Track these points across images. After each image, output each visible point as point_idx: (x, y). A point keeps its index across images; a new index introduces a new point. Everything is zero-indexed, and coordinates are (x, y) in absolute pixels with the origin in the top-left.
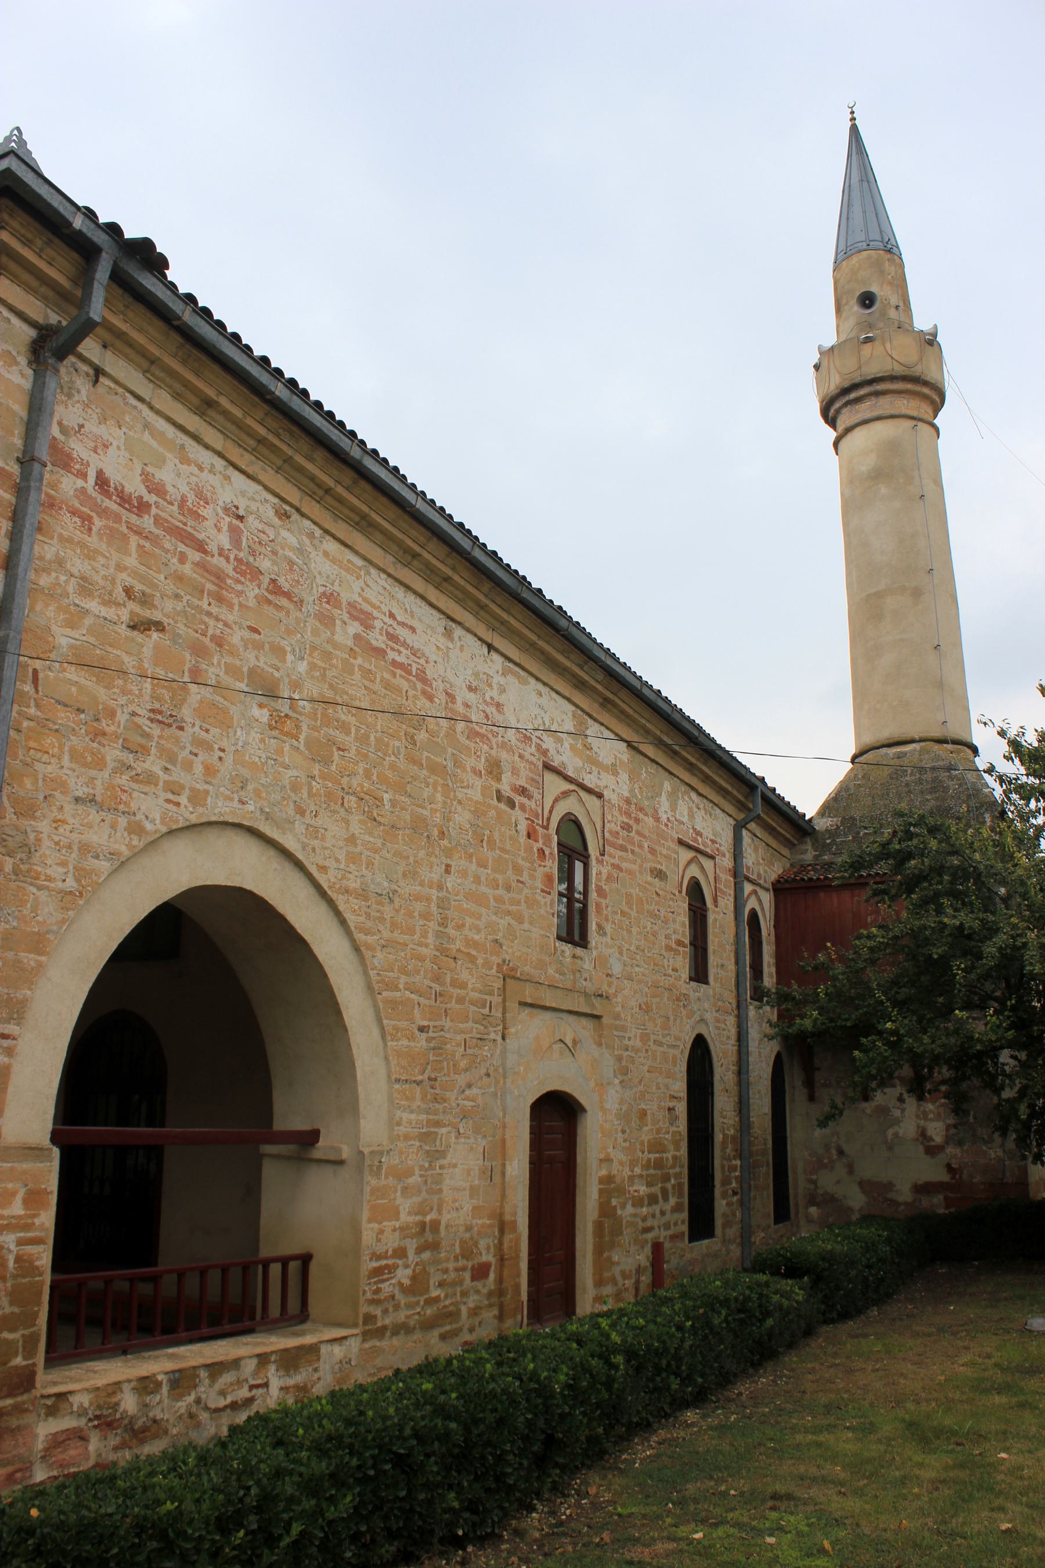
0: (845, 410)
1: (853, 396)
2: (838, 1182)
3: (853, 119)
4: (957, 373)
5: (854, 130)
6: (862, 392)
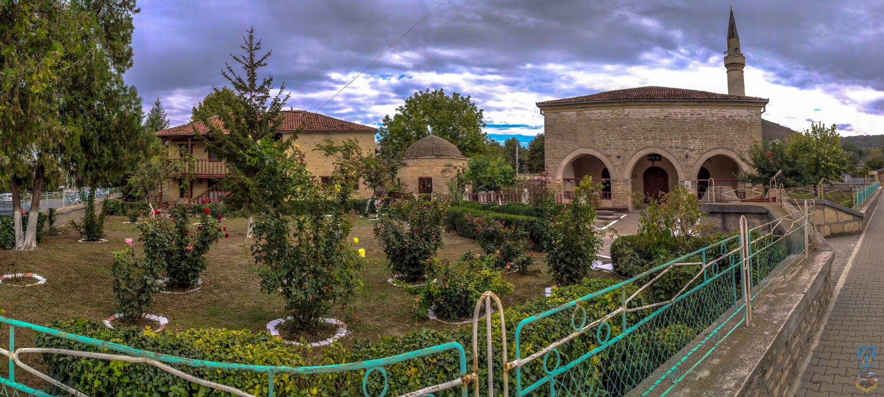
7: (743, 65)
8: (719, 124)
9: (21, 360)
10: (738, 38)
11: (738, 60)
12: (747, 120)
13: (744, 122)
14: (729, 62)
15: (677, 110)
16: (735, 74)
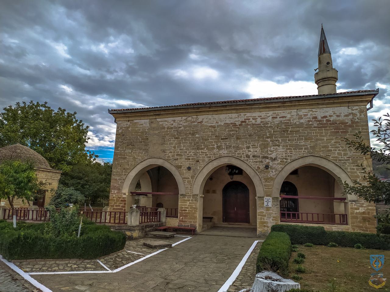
3: (322, 27)
5: (322, 29)
6: (326, 79)
8: (309, 126)
11: (330, 74)
12: (348, 120)
13: (343, 123)
15: (256, 114)
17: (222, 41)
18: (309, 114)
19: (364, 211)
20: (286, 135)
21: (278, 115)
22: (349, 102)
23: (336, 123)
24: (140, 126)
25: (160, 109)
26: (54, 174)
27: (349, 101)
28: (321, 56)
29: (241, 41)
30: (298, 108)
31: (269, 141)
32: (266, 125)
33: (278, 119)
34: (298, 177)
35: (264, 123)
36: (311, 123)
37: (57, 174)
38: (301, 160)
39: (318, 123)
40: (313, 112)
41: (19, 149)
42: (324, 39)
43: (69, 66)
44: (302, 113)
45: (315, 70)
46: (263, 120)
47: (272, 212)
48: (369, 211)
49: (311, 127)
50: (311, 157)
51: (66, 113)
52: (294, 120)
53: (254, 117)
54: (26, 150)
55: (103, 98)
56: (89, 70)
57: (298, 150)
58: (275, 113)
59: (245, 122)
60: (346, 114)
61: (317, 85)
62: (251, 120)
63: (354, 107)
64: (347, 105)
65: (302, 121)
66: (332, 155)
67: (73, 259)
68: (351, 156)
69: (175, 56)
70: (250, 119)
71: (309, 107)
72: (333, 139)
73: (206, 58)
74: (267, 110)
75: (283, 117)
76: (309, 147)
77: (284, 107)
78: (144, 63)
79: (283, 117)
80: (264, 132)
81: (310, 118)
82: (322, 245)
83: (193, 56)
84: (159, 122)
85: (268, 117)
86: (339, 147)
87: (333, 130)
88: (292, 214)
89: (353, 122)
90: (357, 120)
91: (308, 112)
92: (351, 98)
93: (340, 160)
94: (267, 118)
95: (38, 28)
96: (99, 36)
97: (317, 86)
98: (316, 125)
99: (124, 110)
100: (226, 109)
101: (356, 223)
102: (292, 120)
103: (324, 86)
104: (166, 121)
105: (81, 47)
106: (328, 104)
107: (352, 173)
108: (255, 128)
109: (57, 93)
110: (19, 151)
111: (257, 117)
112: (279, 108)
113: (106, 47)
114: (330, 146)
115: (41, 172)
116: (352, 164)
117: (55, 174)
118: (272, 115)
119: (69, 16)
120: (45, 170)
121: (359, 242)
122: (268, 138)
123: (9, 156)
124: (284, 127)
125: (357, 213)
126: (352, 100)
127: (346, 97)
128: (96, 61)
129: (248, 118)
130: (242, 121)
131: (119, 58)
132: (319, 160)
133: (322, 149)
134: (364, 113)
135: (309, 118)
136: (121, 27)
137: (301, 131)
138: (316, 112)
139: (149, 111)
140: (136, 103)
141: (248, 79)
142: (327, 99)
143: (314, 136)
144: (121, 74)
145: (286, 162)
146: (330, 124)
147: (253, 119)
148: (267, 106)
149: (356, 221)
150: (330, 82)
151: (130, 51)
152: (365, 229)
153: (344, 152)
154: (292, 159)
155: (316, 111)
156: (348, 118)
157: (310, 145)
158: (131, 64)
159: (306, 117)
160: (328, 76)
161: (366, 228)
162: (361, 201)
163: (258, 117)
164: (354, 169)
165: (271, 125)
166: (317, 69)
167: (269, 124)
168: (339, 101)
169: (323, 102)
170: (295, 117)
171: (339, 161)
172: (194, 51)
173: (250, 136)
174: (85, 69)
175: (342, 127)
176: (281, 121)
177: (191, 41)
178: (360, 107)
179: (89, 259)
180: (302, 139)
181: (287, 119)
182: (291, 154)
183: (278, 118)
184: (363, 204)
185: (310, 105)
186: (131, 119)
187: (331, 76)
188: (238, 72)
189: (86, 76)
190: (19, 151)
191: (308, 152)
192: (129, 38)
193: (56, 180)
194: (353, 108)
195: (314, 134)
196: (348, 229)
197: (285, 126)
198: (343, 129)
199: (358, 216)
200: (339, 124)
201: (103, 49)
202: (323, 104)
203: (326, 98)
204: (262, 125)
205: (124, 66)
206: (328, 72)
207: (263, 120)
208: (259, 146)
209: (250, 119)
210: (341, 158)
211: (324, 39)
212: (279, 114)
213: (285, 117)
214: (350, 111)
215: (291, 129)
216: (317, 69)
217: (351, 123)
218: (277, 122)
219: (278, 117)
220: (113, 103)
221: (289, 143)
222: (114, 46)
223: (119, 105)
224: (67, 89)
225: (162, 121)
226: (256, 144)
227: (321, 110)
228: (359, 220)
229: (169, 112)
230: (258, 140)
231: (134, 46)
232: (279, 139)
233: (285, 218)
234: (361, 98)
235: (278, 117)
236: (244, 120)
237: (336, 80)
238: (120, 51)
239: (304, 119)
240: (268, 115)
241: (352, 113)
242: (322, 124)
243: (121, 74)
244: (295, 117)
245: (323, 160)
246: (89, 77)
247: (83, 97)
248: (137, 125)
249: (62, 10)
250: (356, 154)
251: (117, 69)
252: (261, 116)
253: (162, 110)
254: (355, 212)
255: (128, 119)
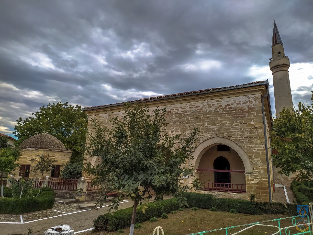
0: (275, 69)
1: (277, 67)
2: (279, 177)
3: (275, 22)
4: (308, 79)
5: (275, 24)
6: (278, 67)
7: (288, 66)
8: (216, 113)
9: (287, 230)
10: (282, 44)
11: (281, 62)
12: (246, 107)
13: (242, 109)
14: (273, 65)
15: (178, 105)
16: (280, 74)
17: (223, 38)
18: (216, 103)
19: (258, 182)
20: (199, 121)
21: (194, 105)
22: (246, 92)
23: (236, 110)
24: (103, 119)
25: (113, 105)
26: (66, 154)
27: (246, 92)
28: (274, 48)
29: (239, 36)
30: (208, 99)
31: (187, 126)
32: (185, 114)
33: (194, 109)
34: (230, 153)
35: (184, 112)
36: (217, 110)
37: (69, 153)
38: (210, 140)
39: (223, 110)
40: (219, 101)
41: (43, 137)
42: (276, 32)
43: (106, 70)
44: (211, 103)
45: (270, 59)
46: (183, 110)
47: (188, 182)
48: (262, 182)
49: (218, 114)
50: (217, 138)
51: (81, 108)
52: (205, 109)
53: (177, 107)
54: (48, 137)
55: (132, 91)
56: (121, 71)
57: (207, 133)
58: (192, 104)
59: (170, 112)
60: (244, 102)
61: (272, 71)
62: (175, 110)
63: (250, 96)
64: (245, 94)
65: (211, 109)
66: (233, 136)
67: (5, 214)
68: (247, 136)
69: (184, 53)
70: (174, 110)
71: (216, 98)
72: (234, 123)
73: (210, 52)
74: (186, 101)
75: (197, 107)
76: (215, 130)
77: (198, 98)
78: (161, 62)
79: (197, 107)
80: (183, 119)
81: (217, 107)
82: (207, 209)
83: (198, 52)
84: (114, 115)
85: (187, 107)
86: (238, 129)
87: (234, 116)
88: (221, 184)
89: (249, 108)
90: (253, 106)
91: (216, 102)
92: (246, 89)
93: (239, 140)
94: (186, 108)
95: (84, 45)
96: (126, 45)
97: (272, 72)
98: (221, 112)
99: (200, 91)
100: (157, 103)
101: (252, 192)
102: (204, 109)
103: (277, 72)
104: (118, 114)
105: (114, 56)
106: (230, 94)
107: (248, 150)
108: (178, 116)
109: (101, 91)
110: (43, 138)
111: (179, 107)
112: (194, 100)
113: (132, 53)
114: (231, 129)
115: (56, 152)
116: (248, 142)
117: (67, 154)
118: (189, 106)
119: (104, 34)
120: (59, 151)
121: (234, 207)
122: (186, 123)
123: (36, 142)
124: (198, 115)
125: (252, 183)
126: (248, 90)
127: (242, 88)
128: (125, 65)
129: (172, 109)
130: (168, 112)
131: (141, 60)
132: (223, 140)
133: (225, 131)
134: (259, 100)
135: (216, 107)
136: (141, 37)
137: (210, 117)
138: (221, 101)
139: (107, 107)
140: (156, 93)
141: (250, 66)
142: (229, 91)
143: (219, 121)
144: (144, 72)
145: (199, 142)
146: (231, 110)
147: (176, 109)
148: (185, 99)
149: (252, 190)
150: (282, 69)
151: (149, 54)
152: (258, 197)
153: (242, 133)
154: (203, 140)
155: (221, 100)
156: (246, 105)
157: (217, 128)
158: (150, 64)
159: (214, 106)
160: (280, 64)
161: (259, 197)
162: (255, 174)
163: (180, 107)
164: (249, 147)
165: (189, 113)
166: (271, 58)
167: (187, 113)
168: (238, 92)
169: (226, 93)
170: (206, 106)
171: (238, 140)
172: (199, 48)
173: (174, 122)
174: (118, 71)
175: (241, 112)
176: (196, 110)
177: (196, 41)
178: (255, 96)
179: (15, 215)
180: (211, 124)
181: (200, 108)
182: (203, 135)
183: (194, 107)
184: (257, 176)
185: (216, 96)
186: (97, 114)
187: (283, 63)
188: (242, 60)
189: (119, 76)
190: (43, 138)
191: (215, 134)
192: (148, 45)
193: (68, 158)
194: (250, 96)
195: (220, 119)
196: (245, 197)
197: (199, 114)
198: (242, 114)
199: (252, 186)
200: (239, 110)
201: (129, 55)
202: (226, 95)
203: (227, 90)
204: (182, 114)
205: (146, 66)
206: (280, 60)
207: (183, 110)
208: (180, 130)
209: (174, 110)
210: (240, 138)
211: (276, 32)
212: (195, 104)
213: (199, 107)
214: (247, 99)
215: (202, 116)
216: (271, 58)
217: (248, 109)
218: (193, 111)
219: (194, 107)
220: (139, 95)
221: (202, 127)
222: (139, 51)
223: (144, 96)
224: (108, 87)
225: (116, 114)
226: (178, 129)
227: (225, 100)
228: (254, 189)
229: (120, 108)
230: (179, 126)
231: (152, 50)
232: (194, 124)
233: (219, 187)
234: (255, 88)
235: (194, 107)
236: (170, 111)
237: (288, 66)
238: (142, 55)
239: (212, 107)
240: (187, 106)
241: (249, 101)
242: (225, 111)
243: (144, 72)
244: (206, 106)
245: (226, 140)
246: (121, 77)
247: (118, 92)
248: (101, 118)
249: (99, 30)
250: (251, 134)
251: (141, 69)
252: (182, 107)
253: (115, 106)
254: (251, 183)
255: (95, 114)
